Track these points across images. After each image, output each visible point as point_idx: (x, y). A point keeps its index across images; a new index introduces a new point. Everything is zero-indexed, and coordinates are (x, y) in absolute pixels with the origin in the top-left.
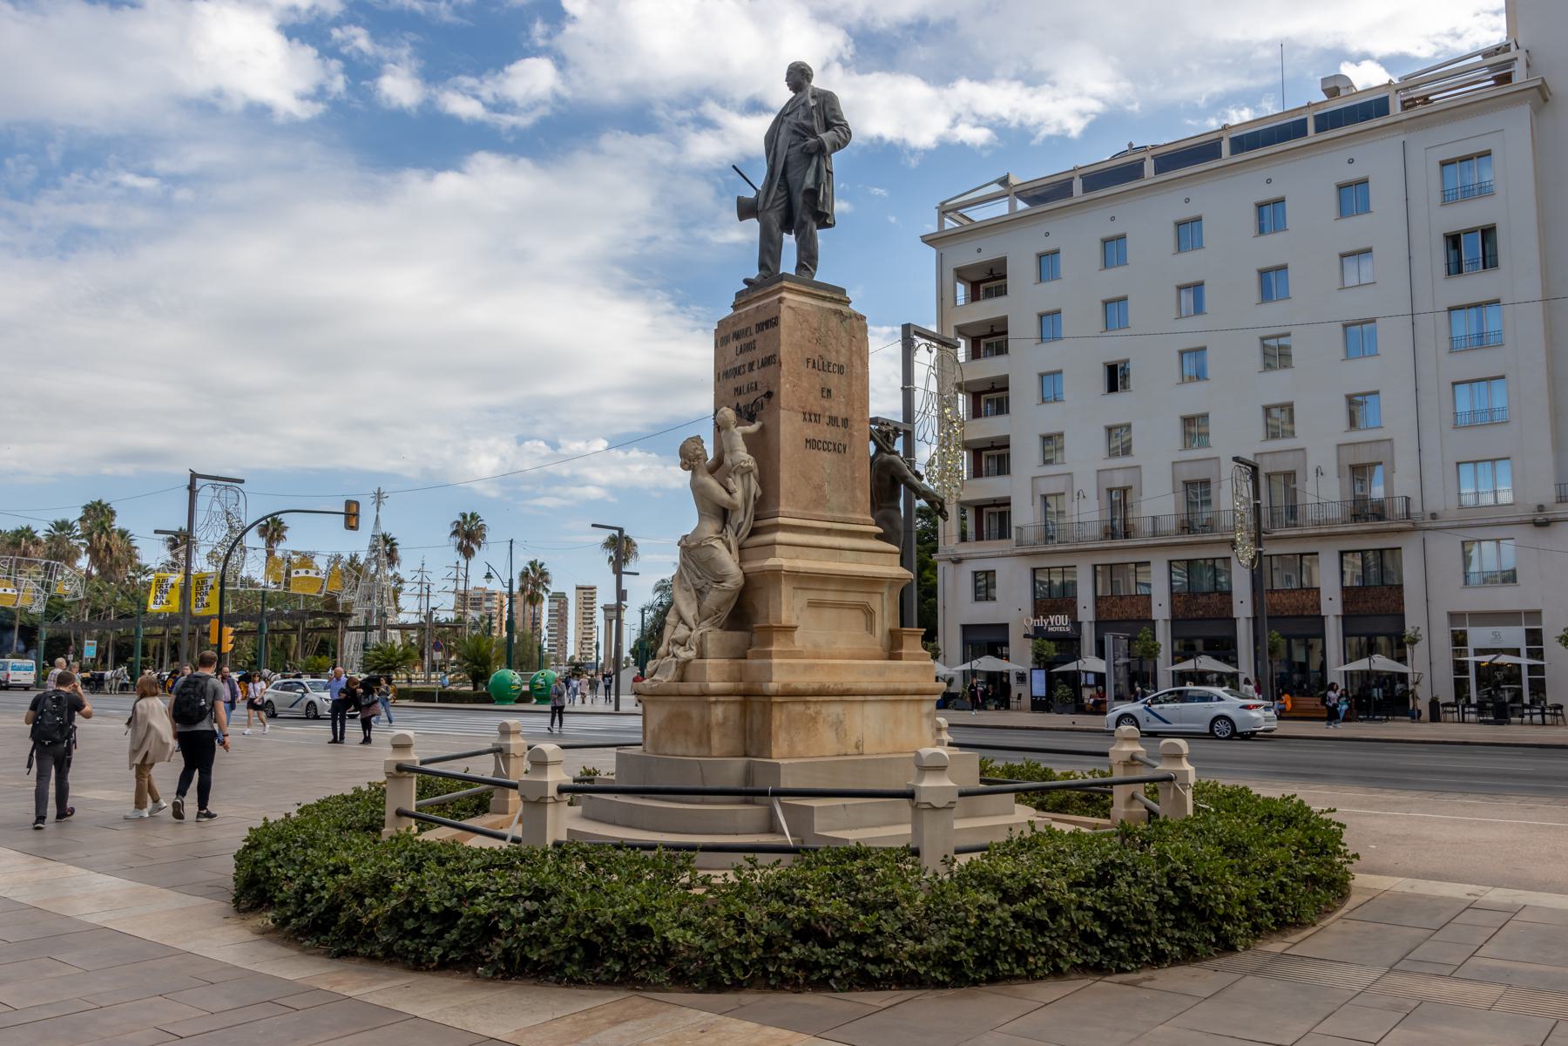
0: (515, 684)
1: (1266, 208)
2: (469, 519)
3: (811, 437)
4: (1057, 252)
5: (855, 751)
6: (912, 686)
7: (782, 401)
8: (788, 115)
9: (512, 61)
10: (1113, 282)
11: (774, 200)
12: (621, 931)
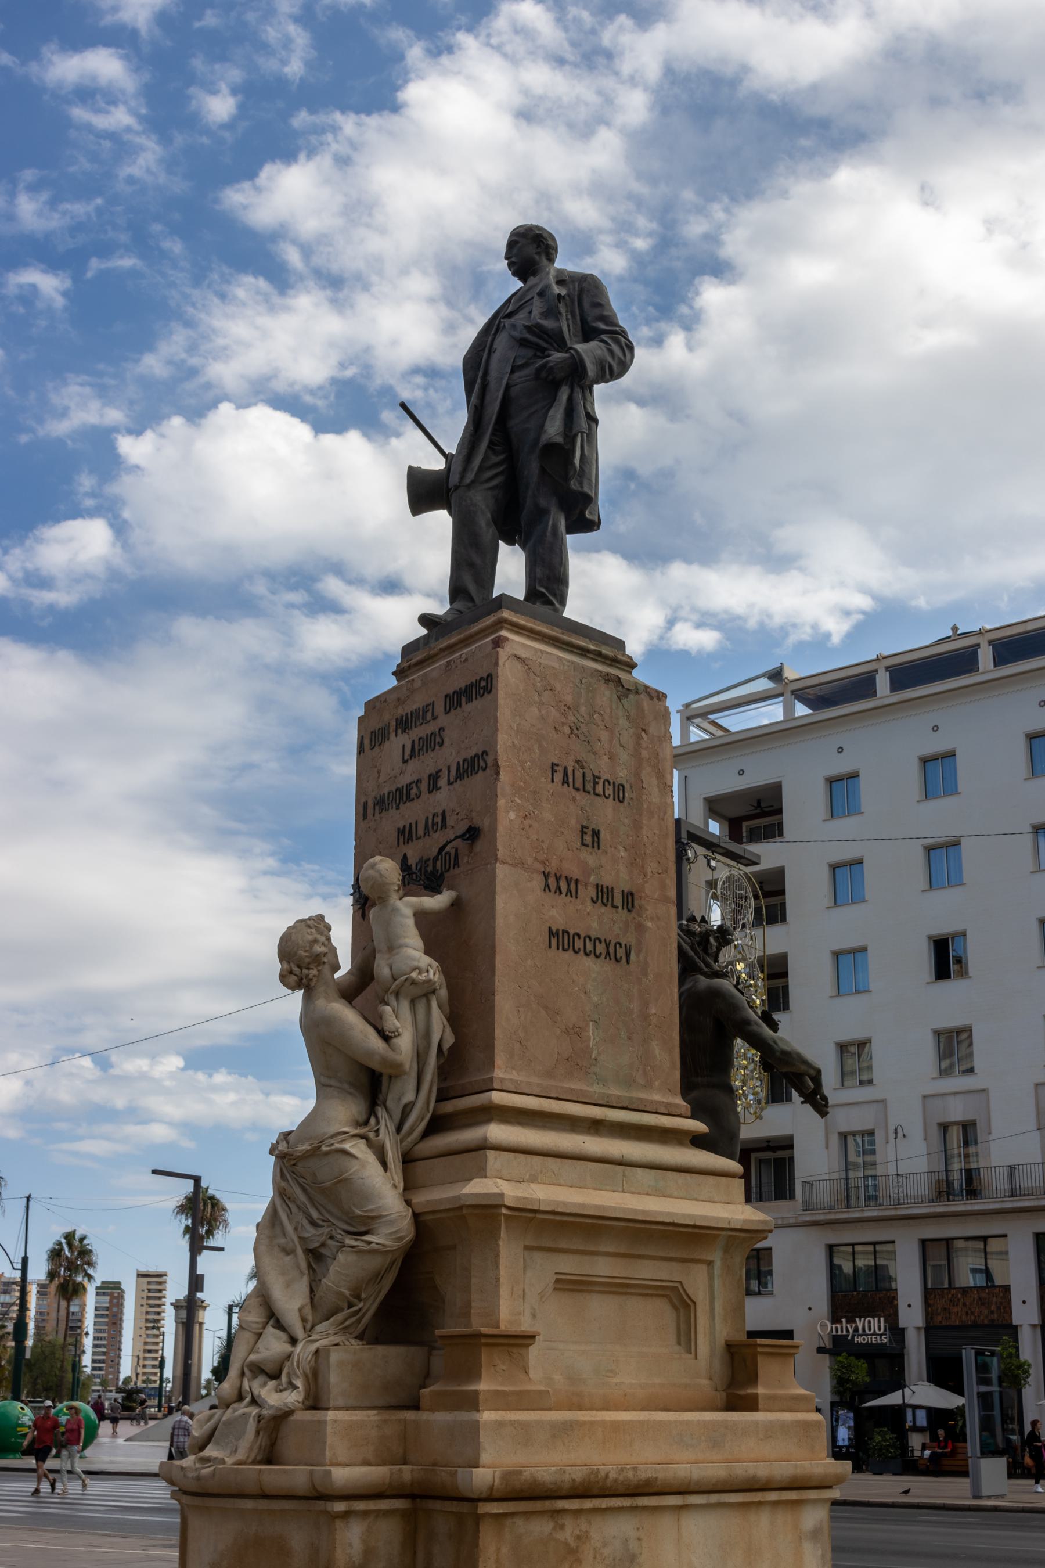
0: (23, 1425)
3: (559, 924)
4: (855, 776)
6: (782, 1471)
7: (500, 846)
8: (510, 315)
9: (58, 518)
11: (481, 469)
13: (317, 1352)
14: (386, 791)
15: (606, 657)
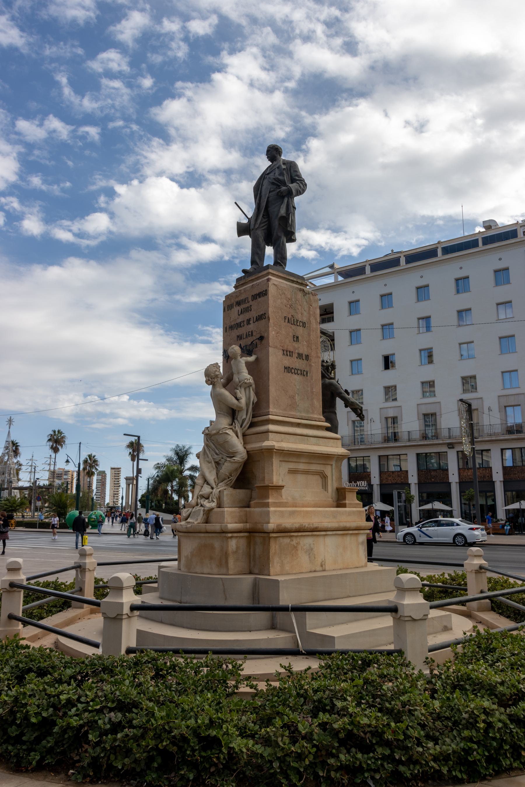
1: (460, 281)
2: (57, 433)
3: (287, 365)
5: (321, 569)
6: (354, 525)
8: (268, 174)
10: (386, 316)
11: (260, 223)
12: (193, 741)
13: (220, 491)
14: (233, 324)
15: (299, 283)
